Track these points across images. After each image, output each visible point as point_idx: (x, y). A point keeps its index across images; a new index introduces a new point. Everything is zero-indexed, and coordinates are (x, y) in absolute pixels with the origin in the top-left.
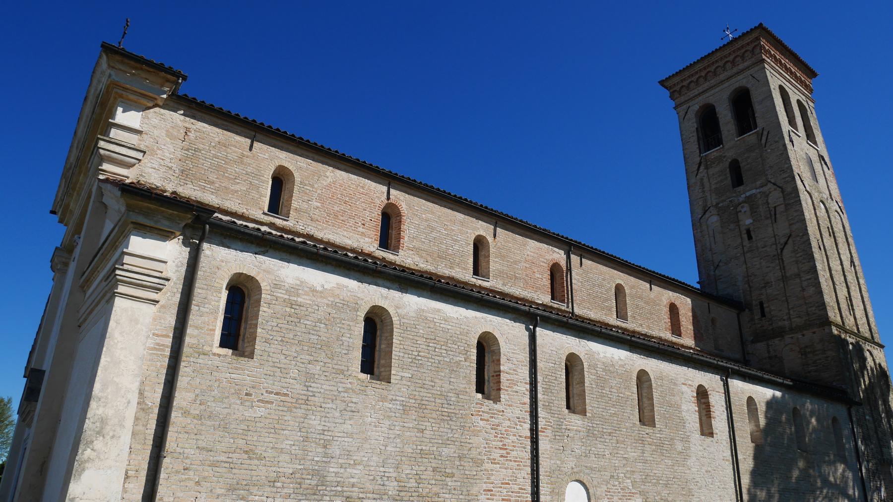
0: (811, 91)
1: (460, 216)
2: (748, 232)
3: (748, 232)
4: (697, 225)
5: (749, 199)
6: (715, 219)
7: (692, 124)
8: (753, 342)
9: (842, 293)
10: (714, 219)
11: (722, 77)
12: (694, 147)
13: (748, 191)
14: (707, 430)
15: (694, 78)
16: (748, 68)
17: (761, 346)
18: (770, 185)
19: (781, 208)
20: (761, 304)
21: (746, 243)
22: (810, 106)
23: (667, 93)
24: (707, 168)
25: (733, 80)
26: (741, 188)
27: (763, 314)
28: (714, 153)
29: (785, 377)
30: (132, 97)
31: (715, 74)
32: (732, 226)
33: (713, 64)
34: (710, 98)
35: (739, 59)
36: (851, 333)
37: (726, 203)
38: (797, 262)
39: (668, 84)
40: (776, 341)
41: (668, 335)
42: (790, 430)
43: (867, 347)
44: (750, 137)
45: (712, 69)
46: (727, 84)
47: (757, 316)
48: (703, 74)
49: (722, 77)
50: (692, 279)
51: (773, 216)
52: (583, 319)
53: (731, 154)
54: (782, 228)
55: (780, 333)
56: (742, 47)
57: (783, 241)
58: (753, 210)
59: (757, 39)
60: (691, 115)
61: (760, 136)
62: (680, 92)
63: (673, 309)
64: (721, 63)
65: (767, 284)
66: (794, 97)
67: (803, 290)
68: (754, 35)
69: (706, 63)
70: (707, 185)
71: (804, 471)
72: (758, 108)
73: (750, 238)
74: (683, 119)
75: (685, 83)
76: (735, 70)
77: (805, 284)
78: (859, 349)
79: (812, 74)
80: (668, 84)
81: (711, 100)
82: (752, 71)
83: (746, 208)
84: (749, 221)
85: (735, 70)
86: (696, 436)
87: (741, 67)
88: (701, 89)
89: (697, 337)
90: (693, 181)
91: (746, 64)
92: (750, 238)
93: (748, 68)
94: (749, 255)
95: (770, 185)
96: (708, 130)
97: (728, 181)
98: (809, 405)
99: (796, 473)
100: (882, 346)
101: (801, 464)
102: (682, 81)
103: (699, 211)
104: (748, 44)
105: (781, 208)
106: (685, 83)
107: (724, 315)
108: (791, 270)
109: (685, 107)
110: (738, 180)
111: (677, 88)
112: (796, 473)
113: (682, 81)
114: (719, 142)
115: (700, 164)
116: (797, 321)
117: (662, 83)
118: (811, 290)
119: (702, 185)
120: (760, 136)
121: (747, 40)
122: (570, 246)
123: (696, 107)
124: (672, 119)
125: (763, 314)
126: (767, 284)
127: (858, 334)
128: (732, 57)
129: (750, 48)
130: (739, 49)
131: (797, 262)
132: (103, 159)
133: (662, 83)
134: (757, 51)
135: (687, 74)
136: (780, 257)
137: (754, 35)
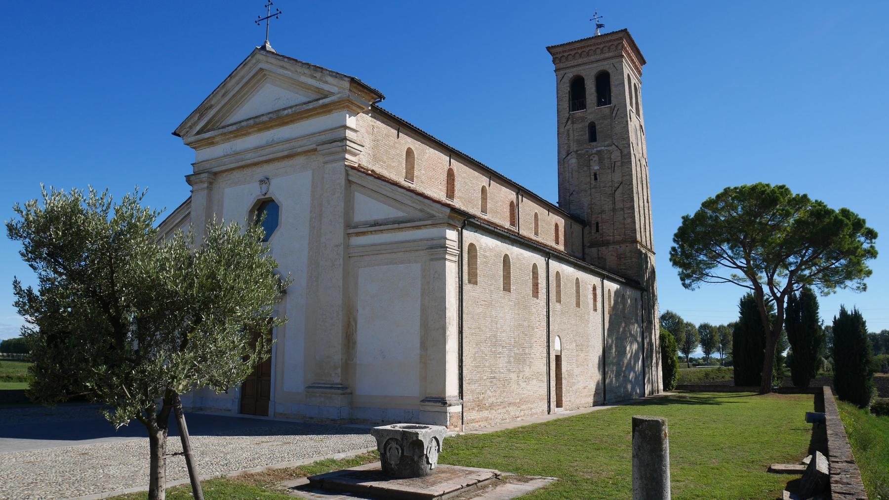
0: (640, 74)
1: (476, 174)
2: (595, 175)
3: (595, 175)
4: (561, 162)
5: (599, 153)
6: (574, 161)
7: (566, 88)
8: (589, 247)
9: (643, 222)
10: (573, 161)
11: (593, 58)
12: (566, 105)
13: (598, 146)
14: (536, 293)
15: (573, 53)
16: (612, 58)
17: (594, 250)
18: (614, 146)
19: (618, 164)
20: (597, 224)
21: (593, 182)
22: (639, 86)
23: (551, 58)
24: (573, 123)
25: (600, 63)
26: (594, 144)
27: (597, 230)
28: (579, 113)
29: (622, 277)
30: (354, 108)
31: (588, 54)
32: (585, 168)
33: (588, 46)
34: (582, 71)
35: (606, 49)
36: (646, 247)
37: (583, 152)
38: (623, 201)
39: (553, 51)
40: (604, 248)
41: (507, 225)
42: (621, 307)
43: (649, 254)
44: (605, 109)
45: (587, 50)
46: (595, 65)
47: (594, 231)
48: (580, 51)
49: (593, 58)
50: (554, 200)
51: (613, 168)
52: (523, 237)
53: (591, 118)
54: (617, 177)
55: (607, 244)
56: (610, 41)
57: (616, 185)
58: (601, 161)
59: (621, 39)
60: (567, 80)
61: (612, 110)
62: (560, 60)
63: (557, 226)
64: (593, 48)
65: (603, 212)
66: (633, 82)
67: (625, 219)
68: (620, 35)
69: (583, 44)
70: (571, 135)
71: (624, 328)
72: (614, 90)
73: (596, 179)
74: (559, 82)
75: (566, 54)
76: (602, 56)
77: (626, 215)
78: (646, 255)
79: (643, 62)
80: (553, 51)
81: (583, 74)
82: (614, 61)
83: (596, 158)
84: (596, 168)
85: (602, 56)
86: (592, 311)
87: (607, 55)
88: (575, 62)
89: (566, 245)
90: (562, 130)
91: (611, 54)
92: (596, 179)
93: (612, 58)
94: (593, 190)
95: (614, 146)
96: (576, 93)
97: (587, 136)
98: (629, 292)
99: (621, 330)
100: (654, 254)
101: (623, 325)
102: (563, 52)
103: (564, 153)
104: (615, 40)
105: (618, 164)
106: (566, 54)
107: (577, 228)
108: (619, 205)
109: (562, 72)
110: (593, 137)
111: (559, 56)
112: (621, 330)
113: (563, 52)
114: (582, 106)
115: (569, 118)
116: (617, 238)
117: (548, 49)
118: (629, 220)
119: (568, 134)
120: (612, 110)
121: (615, 37)
122: (521, 191)
123: (571, 75)
124: (552, 79)
125: (597, 230)
126: (603, 212)
127: (646, 247)
128: (602, 46)
129: (615, 43)
130: (608, 42)
131: (623, 201)
132: (346, 151)
133: (548, 49)
134: (620, 47)
135: (568, 48)
136: (613, 195)
137: (620, 35)
